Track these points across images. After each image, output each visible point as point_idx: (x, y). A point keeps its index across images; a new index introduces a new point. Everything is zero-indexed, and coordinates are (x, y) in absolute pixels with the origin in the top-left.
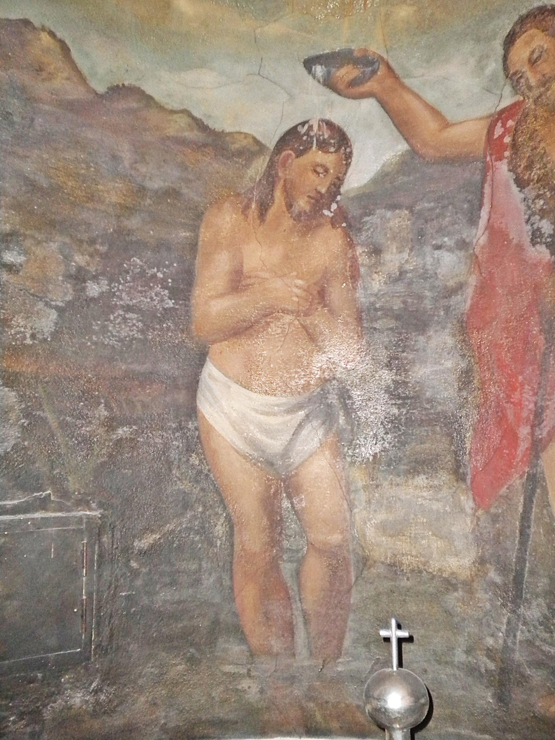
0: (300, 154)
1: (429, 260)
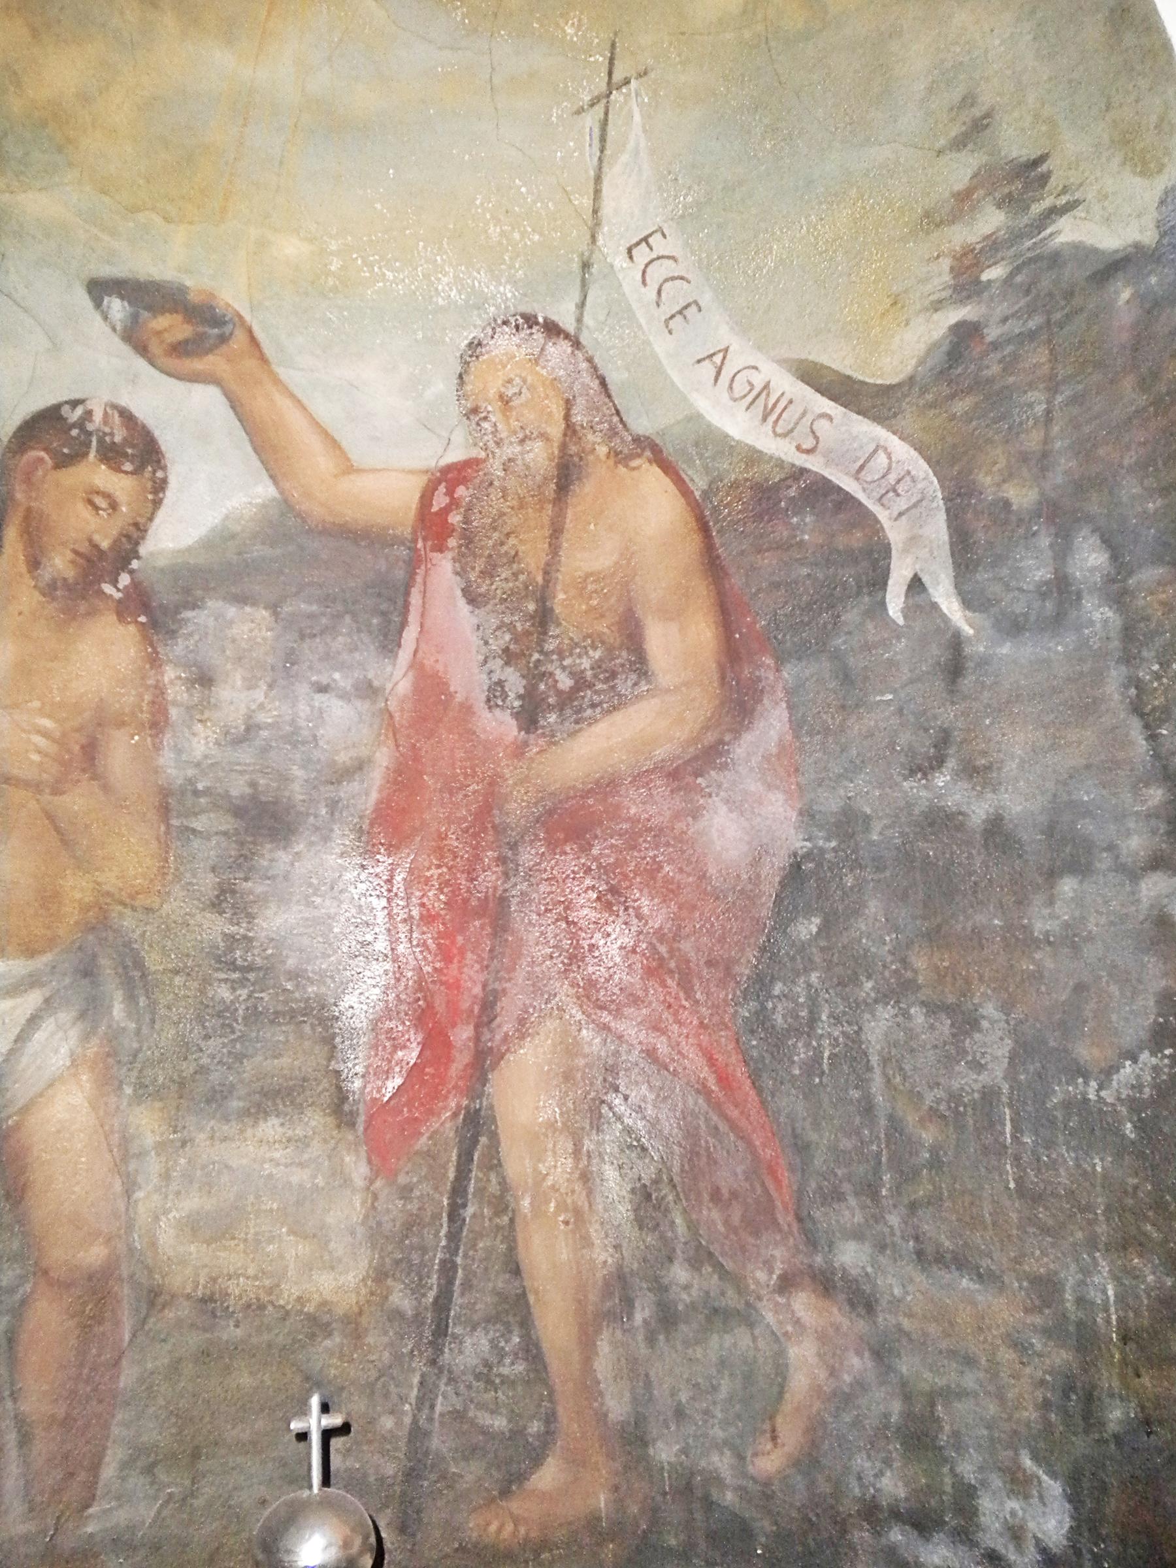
0: (63, 462)
1: (303, 709)
